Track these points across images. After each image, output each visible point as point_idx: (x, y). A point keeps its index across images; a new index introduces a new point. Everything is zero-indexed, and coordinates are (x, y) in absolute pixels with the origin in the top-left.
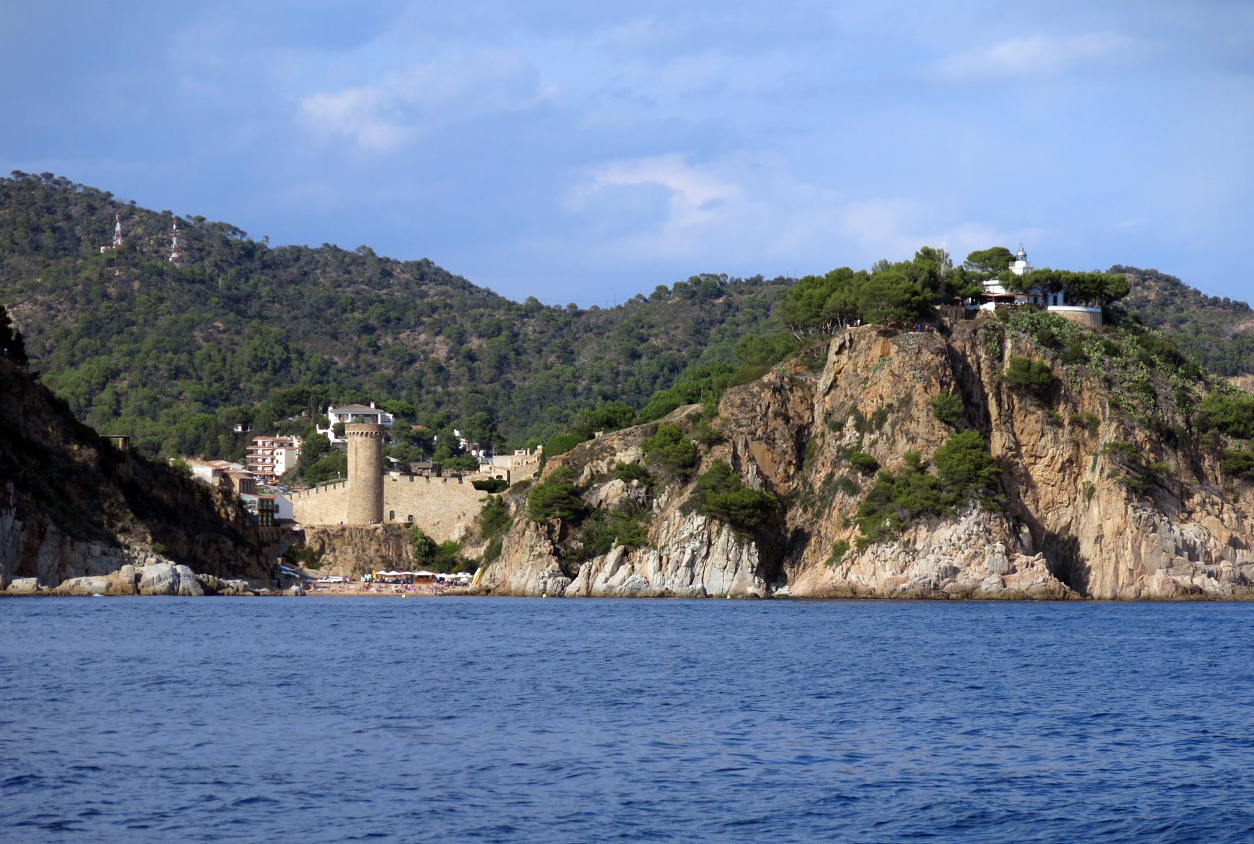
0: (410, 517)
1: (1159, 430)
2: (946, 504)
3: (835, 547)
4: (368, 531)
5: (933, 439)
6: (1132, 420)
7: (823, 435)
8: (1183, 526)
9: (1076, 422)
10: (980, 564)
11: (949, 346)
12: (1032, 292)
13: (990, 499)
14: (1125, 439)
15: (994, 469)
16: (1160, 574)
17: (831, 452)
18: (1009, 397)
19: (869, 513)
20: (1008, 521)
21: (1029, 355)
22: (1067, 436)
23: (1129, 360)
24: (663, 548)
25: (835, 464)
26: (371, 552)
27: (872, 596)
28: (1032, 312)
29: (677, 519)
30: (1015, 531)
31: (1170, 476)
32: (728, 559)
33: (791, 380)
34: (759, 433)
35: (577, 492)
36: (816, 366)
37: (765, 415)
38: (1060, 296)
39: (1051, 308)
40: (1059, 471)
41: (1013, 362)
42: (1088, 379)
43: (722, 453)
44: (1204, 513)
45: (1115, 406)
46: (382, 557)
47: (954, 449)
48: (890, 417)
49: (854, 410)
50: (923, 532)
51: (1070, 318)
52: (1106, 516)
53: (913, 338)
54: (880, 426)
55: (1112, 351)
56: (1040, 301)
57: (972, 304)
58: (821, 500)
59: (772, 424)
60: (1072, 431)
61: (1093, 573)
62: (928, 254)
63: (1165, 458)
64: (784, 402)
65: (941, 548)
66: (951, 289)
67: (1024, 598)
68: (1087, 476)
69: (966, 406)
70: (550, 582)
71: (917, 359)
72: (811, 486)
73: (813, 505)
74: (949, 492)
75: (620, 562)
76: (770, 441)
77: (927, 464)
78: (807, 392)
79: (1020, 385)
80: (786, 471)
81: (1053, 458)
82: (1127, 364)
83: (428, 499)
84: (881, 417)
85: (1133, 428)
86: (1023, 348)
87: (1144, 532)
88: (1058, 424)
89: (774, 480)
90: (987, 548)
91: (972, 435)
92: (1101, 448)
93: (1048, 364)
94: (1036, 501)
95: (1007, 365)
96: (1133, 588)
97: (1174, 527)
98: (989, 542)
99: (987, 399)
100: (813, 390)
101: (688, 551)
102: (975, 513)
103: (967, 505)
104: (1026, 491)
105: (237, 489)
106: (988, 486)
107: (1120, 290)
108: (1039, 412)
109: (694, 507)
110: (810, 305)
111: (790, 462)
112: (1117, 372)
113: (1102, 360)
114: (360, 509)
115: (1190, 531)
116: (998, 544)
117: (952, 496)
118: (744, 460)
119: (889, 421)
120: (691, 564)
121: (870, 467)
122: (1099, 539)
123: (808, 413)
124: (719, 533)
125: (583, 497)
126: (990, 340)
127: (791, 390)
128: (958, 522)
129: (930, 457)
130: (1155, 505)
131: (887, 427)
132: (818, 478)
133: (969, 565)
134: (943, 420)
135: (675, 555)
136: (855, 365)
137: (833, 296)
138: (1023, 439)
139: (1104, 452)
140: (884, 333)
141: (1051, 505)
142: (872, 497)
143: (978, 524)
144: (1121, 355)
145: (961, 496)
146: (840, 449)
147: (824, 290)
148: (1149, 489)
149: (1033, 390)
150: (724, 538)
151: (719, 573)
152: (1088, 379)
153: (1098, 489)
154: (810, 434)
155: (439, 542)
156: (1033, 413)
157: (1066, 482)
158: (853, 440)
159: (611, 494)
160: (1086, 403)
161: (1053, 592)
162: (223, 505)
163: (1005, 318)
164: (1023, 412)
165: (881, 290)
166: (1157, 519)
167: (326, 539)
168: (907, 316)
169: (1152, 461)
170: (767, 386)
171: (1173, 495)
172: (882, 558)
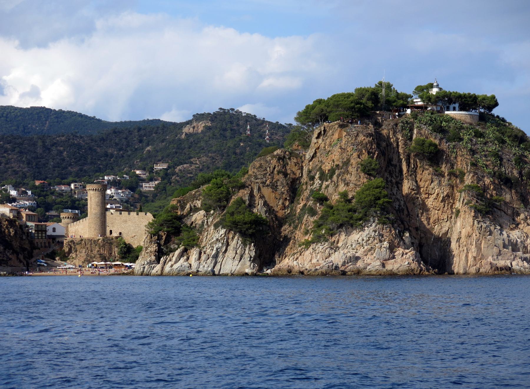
0: (120, 233)
2: (356, 220)
4: (95, 241)
6: (484, 172)
8: (511, 232)
13: (383, 216)
14: (478, 183)
17: (306, 193)
18: (414, 161)
20: (395, 229)
23: (489, 140)
24: (203, 247)
25: (308, 199)
26: (95, 252)
29: (212, 231)
30: (400, 235)
31: (506, 203)
32: (236, 253)
34: (268, 182)
35: (180, 218)
36: (306, 146)
37: (273, 172)
38: (457, 105)
39: (446, 112)
40: (442, 201)
43: (244, 194)
44: (526, 224)
45: (474, 165)
46: (100, 254)
48: (337, 172)
49: (320, 168)
50: (343, 237)
51: (458, 117)
52: (463, 227)
54: (331, 177)
58: (298, 220)
59: (276, 177)
60: (449, 180)
61: (455, 259)
64: (284, 166)
65: (352, 245)
67: (392, 276)
68: (458, 205)
70: (147, 267)
71: (356, 139)
73: (294, 222)
75: (181, 255)
76: (274, 187)
80: (283, 204)
81: (438, 194)
83: (130, 223)
84: (332, 172)
86: (423, 133)
88: (442, 175)
89: (276, 209)
93: (437, 142)
94: (428, 219)
97: (504, 233)
99: (401, 162)
101: (215, 249)
102: (374, 225)
103: (369, 221)
104: (422, 213)
105: (24, 219)
108: (431, 169)
109: (221, 224)
111: (286, 199)
114: (93, 230)
115: (515, 235)
118: (257, 198)
119: (336, 174)
120: (216, 256)
121: (323, 200)
122: (459, 239)
123: (299, 171)
124: (233, 238)
125: (184, 220)
126: (405, 129)
127: (289, 159)
131: (335, 178)
133: (366, 255)
135: (208, 251)
138: (422, 184)
139: (465, 191)
143: (375, 231)
144: (484, 137)
145: (366, 215)
148: (489, 210)
150: (236, 241)
151: (230, 261)
153: (461, 211)
154: (300, 183)
155: (135, 246)
156: (427, 169)
157: (446, 208)
159: (198, 218)
160: (459, 163)
161: (413, 270)
162: (7, 228)
166: (492, 228)
167: (73, 245)
170: (274, 156)
172: (317, 252)
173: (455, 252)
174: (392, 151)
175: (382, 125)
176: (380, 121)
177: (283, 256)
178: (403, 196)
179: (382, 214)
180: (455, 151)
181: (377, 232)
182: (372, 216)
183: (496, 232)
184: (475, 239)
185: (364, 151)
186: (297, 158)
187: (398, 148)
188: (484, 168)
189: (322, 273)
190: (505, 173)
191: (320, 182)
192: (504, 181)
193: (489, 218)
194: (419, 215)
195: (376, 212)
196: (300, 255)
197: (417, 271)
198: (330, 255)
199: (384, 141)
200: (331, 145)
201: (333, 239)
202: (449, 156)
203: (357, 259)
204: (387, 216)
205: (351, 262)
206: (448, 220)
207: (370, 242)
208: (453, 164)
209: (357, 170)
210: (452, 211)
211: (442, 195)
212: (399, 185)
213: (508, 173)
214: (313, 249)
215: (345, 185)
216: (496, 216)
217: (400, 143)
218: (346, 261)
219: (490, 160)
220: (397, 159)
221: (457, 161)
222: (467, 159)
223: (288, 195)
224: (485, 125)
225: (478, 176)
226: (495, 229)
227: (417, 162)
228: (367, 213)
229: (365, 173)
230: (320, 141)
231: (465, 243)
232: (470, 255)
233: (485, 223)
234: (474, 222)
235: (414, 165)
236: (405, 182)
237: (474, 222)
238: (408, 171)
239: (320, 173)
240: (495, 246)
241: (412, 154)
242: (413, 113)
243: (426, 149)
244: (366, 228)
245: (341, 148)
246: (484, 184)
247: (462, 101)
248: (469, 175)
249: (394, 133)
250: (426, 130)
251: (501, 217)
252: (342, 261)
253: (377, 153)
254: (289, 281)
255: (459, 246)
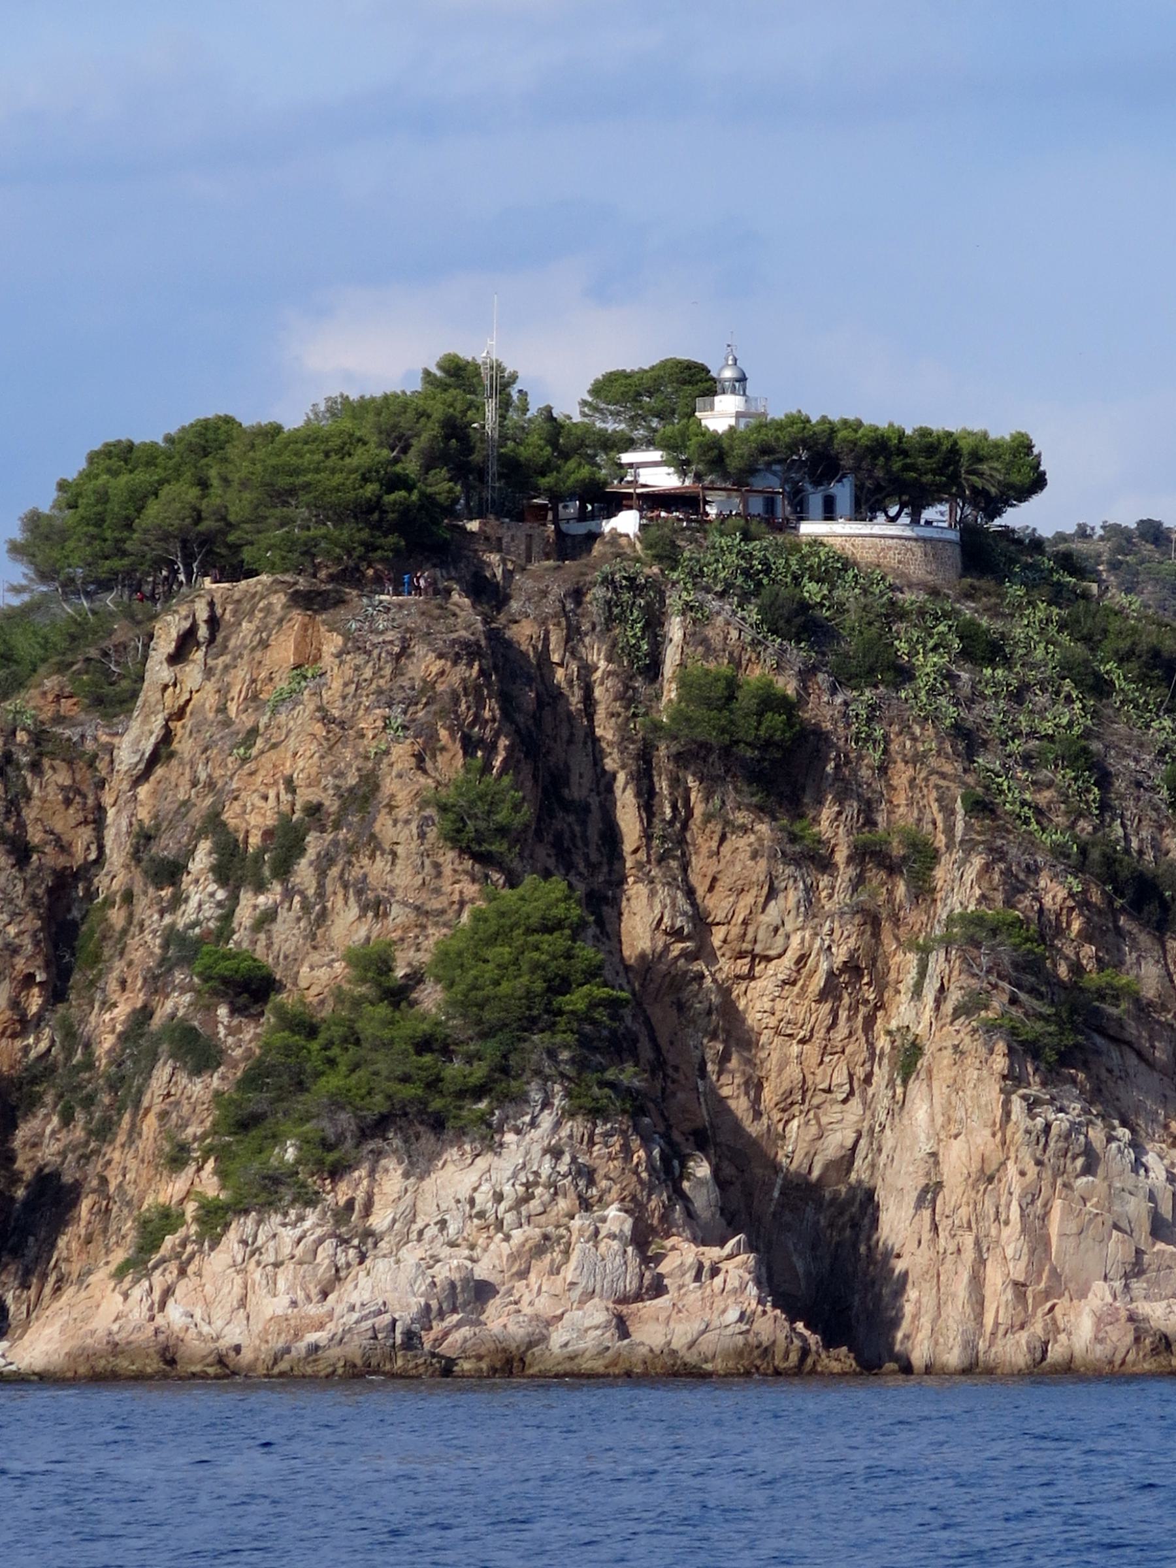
1: (1112, 878)
2: (461, 1094)
3: (144, 1224)
5: (435, 904)
6: (1031, 845)
7: (128, 897)
9: (868, 854)
10: (555, 1271)
11: (495, 636)
12: (759, 483)
13: (591, 1077)
14: (1009, 903)
15: (604, 992)
16: (1100, 1294)
17: (144, 948)
18: (675, 782)
19: (245, 1124)
20: (646, 1143)
21: (736, 663)
22: (842, 897)
25: (157, 983)
27: (225, 1369)
28: (747, 537)
30: (669, 1174)
31: (1143, 1008)
33: (39, 737)
36: (114, 698)
38: (843, 492)
40: (822, 996)
41: (684, 682)
42: (906, 729)
45: (982, 807)
47: (493, 931)
48: (314, 843)
49: (214, 823)
50: (392, 1179)
51: (864, 555)
53: (387, 611)
54: (283, 869)
55: (983, 649)
56: (783, 509)
57: (583, 516)
58: (113, 1087)
60: (858, 883)
61: (912, 1294)
62: (457, 373)
63: (1130, 958)
65: (443, 1224)
66: (517, 473)
67: (679, 1372)
68: (906, 1013)
69: (541, 804)
71: (397, 672)
72: (87, 1046)
73: (89, 1102)
74: (469, 1059)
77: (415, 978)
78: (83, 773)
79: (703, 745)
81: (802, 960)
82: (1025, 687)
84: (287, 842)
85: (1033, 871)
86: (717, 642)
87: (1058, 1172)
90: (576, 1223)
91: (546, 894)
92: (938, 931)
93: (788, 685)
94: (754, 1086)
95: (671, 692)
96: (1023, 1337)
97: (1150, 1159)
98: (585, 1205)
99: (610, 789)
100: (102, 766)
102: (547, 1120)
103: (522, 1099)
104: (725, 1058)
106: (584, 1042)
107: (1015, 478)
108: (763, 828)
110: (99, 522)
111: (29, 979)
112: (992, 709)
113: (950, 676)
116: (613, 1212)
117: (479, 1072)
119: (311, 853)
121: (251, 989)
122: (929, 1194)
123: (86, 833)
126: (622, 619)
128: (496, 1148)
129: (425, 957)
130: (1096, 1095)
131: (304, 872)
132: (106, 1025)
133: (523, 1274)
134: (465, 851)
136: (223, 691)
137: (165, 490)
138: (717, 905)
139: (947, 942)
140: (309, 601)
141: (799, 1097)
142: (254, 1079)
143: (556, 1153)
144: (1008, 662)
145: (505, 1070)
146: (171, 937)
147: (142, 477)
148: (1069, 1041)
149: (743, 763)
152: (906, 729)
153: (929, 1049)
154: (91, 895)
156: (745, 830)
157: (842, 1030)
158: (209, 911)
160: (901, 799)
161: (766, 1352)
163: (668, 556)
164: (716, 827)
165: (296, 472)
166: (1096, 1134)
168: (371, 547)
169: (1090, 965)
171: (1151, 1064)
172: (269, 1257)
173: (911, 1261)
174: (564, 733)
175: (507, 598)
176: (499, 572)
177: (44, 1277)
178: (627, 968)
179: (581, 1064)
180: (878, 733)
181: (567, 1158)
182: (538, 1073)
183: (1117, 1157)
184: (1017, 1192)
185: (443, 734)
186: (70, 763)
187: (591, 717)
188: (1027, 822)
189: (350, 1365)
190: (1127, 851)
191: (221, 895)
192: (1129, 892)
193: (1073, 1081)
194: (710, 1067)
195: (552, 1054)
196: (182, 1272)
197: (786, 1357)
198: (337, 1276)
199: (530, 680)
200: (255, 698)
201: (343, 1192)
202: (848, 762)
203: (482, 1291)
204: (610, 1075)
205: (454, 1310)
206: (851, 1093)
207: (534, 1206)
208: (869, 802)
209: (422, 836)
210: (871, 1046)
211: (824, 966)
212: (607, 910)
213: (1141, 852)
214: (244, 1243)
215: (364, 909)
216: (1104, 1074)
217: (598, 692)
218: (434, 1304)
219: (1050, 785)
220: (589, 774)
221: (891, 788)
222: (943, 776)
223: (40, 961)
224: (1002, 596)
225: (1009, 869)
226: (1110, 1139)
227: (688, 790)
228: (514, 1060)
229: (462, 851)
230: (192, 673)
231: (964, 1212)
232: (994, 1277)
233: (1061, 1110)
234: (1007, 1103)
235: (674, 808)
236: (636, 894)
237: (1007, 1103)
238: (647, 836)
239: (217, 848)
240: (1116, 1227)
241: (663, 751)
242: (654, 532)
243: (746, 729)
244: (510, 1137)
245: (325, 718)
246: (1041, 911)
247: (888, 471)
248: (965, 861)
249: (568, 639)
250: (731, 623)
251: (1125, 1076)
252: (416, 1303)
253: (503, 742)
254: (438, 1402)
255: (935, 1228)
